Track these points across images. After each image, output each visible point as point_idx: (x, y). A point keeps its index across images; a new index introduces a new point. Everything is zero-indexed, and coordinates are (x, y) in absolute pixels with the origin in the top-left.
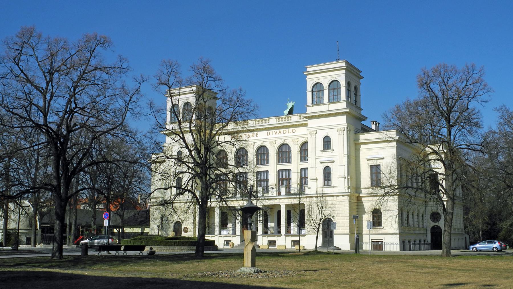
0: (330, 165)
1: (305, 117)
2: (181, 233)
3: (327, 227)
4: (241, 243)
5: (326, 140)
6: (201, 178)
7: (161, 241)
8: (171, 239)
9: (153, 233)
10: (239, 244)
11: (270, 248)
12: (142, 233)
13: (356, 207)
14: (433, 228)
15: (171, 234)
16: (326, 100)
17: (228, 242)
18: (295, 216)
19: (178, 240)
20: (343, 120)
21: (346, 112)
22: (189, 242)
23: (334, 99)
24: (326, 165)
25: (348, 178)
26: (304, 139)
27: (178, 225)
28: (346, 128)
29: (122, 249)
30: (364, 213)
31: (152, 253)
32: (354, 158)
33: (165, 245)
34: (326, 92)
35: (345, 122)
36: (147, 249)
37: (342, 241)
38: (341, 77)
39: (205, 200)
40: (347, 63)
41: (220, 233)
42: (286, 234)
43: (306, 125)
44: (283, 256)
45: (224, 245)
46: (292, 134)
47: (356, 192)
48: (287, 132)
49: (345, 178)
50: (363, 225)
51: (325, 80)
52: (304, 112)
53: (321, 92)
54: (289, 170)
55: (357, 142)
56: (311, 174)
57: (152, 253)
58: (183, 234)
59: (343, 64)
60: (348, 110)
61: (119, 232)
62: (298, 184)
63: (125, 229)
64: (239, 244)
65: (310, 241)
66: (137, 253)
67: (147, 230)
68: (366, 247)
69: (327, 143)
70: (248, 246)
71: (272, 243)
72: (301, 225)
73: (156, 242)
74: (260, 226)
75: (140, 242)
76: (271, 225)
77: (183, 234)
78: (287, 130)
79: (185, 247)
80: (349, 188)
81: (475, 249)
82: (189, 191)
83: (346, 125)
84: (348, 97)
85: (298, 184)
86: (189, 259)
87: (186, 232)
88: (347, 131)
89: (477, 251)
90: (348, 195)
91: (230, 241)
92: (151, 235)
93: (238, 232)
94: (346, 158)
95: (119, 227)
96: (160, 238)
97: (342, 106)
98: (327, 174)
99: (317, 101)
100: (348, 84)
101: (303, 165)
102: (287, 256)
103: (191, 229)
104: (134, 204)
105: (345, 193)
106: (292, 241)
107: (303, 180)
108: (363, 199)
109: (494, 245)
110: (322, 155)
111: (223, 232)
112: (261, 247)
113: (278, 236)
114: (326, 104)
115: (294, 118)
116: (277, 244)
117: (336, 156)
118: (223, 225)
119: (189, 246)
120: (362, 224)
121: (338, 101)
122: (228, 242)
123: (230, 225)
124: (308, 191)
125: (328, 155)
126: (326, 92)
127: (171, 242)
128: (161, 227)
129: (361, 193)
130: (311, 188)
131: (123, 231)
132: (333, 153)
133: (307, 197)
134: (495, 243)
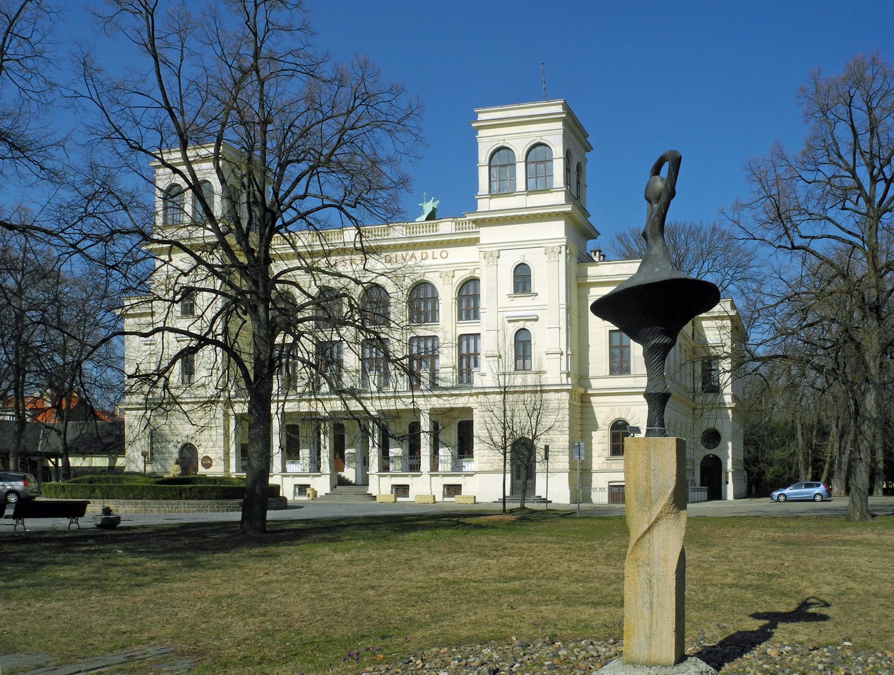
0: (528, 325)
1: (475, 222)
2: (196, 469)
3: (522, 457)
4: (332, 489)
5: (520, 273)
6: (252, 309)
7: (143, 487)
8: (171, 481)
9: (132, 468)
10: (328, 491)
11: (399, 499)
12: (111, 468)
13: (579, 415)
14: (706, 458)
15: (173, 470)
16: (521, 185)
17: (302, 489)
18: (451, 435)
19: (187, 484)
20: (557, 230)
21: (565, 213)
22: (220, 490)
23: (539, 182)
24: (520, 325)
25: (567, 355)
26: (467, 272)
27: (188, 453)
28: (563, 248)
29: (9, 511)
30: (595, 427)
31: (110, 522)
32: (577, 313)
33: (155, 498)
34: (520, 169)
35: (563, 235)
36: (95, 508)
37: (553, 487)
38: (554, 136)
39: (266, 371)
40: (566, 106)
41: (284, 470)
42: (380, 471)
43: (475, 242)
44: (480, 527)
45: (295, 494)
46: (440, 261)
47: (582, 386)
48: (430, 255)
49: (562, 354)
50: (593, 453)
51: (518, 142)
52: (473, 208)
53: (548, 164)
54: (477, 336)
55: (582, 281)
56: (486, 345)
57: (110, 522)
58: (201, 470)
59: (559, 109)
60: (568, 208)
61: (56, 465)
62: (454, 367)
63: (70, 459)
64: (328, 491)
65: (484, 482)
66: (63, 523)
67: (120, 462)
68: (600, 497)
69: (522, 279)
70: (658, 534)
71: (402, 490)
72: (465, 448)
73: (132, 488)
74: (374, 455)
75: (115, 483)
76: (395, 451)
77: (201, 470)
78: (430, 252)
79: (208, 501)
80: (568, 375)
81: (782, 498)
82: (216, 343)
83: (564, 242)
84: (567, 182)
85: (454, 367)
86: (221, 547)
87: (208, 466)
88: (567, 254)
89: (786, 500)
90: (567, 390)
91: (308, 486)
92: (128, 473)
93: (325, 467)
94: (563, 312)
95: (56, 455)
96: (142, 479)
97: (557, 199)
98: (522, 343)
99: (502, 186)
100: (568, 156)
101: (468, 328)
102: (480, 527)
103: (219, 458)
104: (87, 411)
105: (561, 385)
106: (445, 486)
107: (467, 360)
108: (593, 399)
109: (817, 490)
110: (512, 304)
111: (291, 468)
112: (379, 500)
113: (413, 476)
114: (520, 194)
115: (446, 227)
116: (464, 491)
117: (542, 308)
118: (291, 452)
119: (217, 498)
120: (591, 451)
121: (547, 189)
122: (302, 489)
123: (304, 453)
124: (477, 381)
125: (523, 305)
126: (520, 169)
127: (170, 489)
128: (150, 456)
129: (590, 386)
130: (486, 375)
131: (66, 463)
132: (536, 301)
133: (477, 394)
134: (818, 485)
